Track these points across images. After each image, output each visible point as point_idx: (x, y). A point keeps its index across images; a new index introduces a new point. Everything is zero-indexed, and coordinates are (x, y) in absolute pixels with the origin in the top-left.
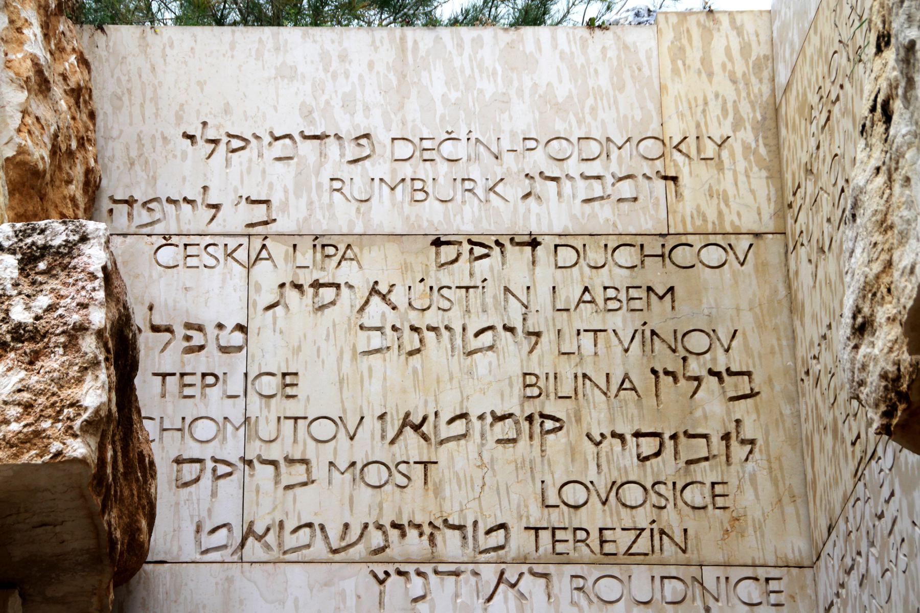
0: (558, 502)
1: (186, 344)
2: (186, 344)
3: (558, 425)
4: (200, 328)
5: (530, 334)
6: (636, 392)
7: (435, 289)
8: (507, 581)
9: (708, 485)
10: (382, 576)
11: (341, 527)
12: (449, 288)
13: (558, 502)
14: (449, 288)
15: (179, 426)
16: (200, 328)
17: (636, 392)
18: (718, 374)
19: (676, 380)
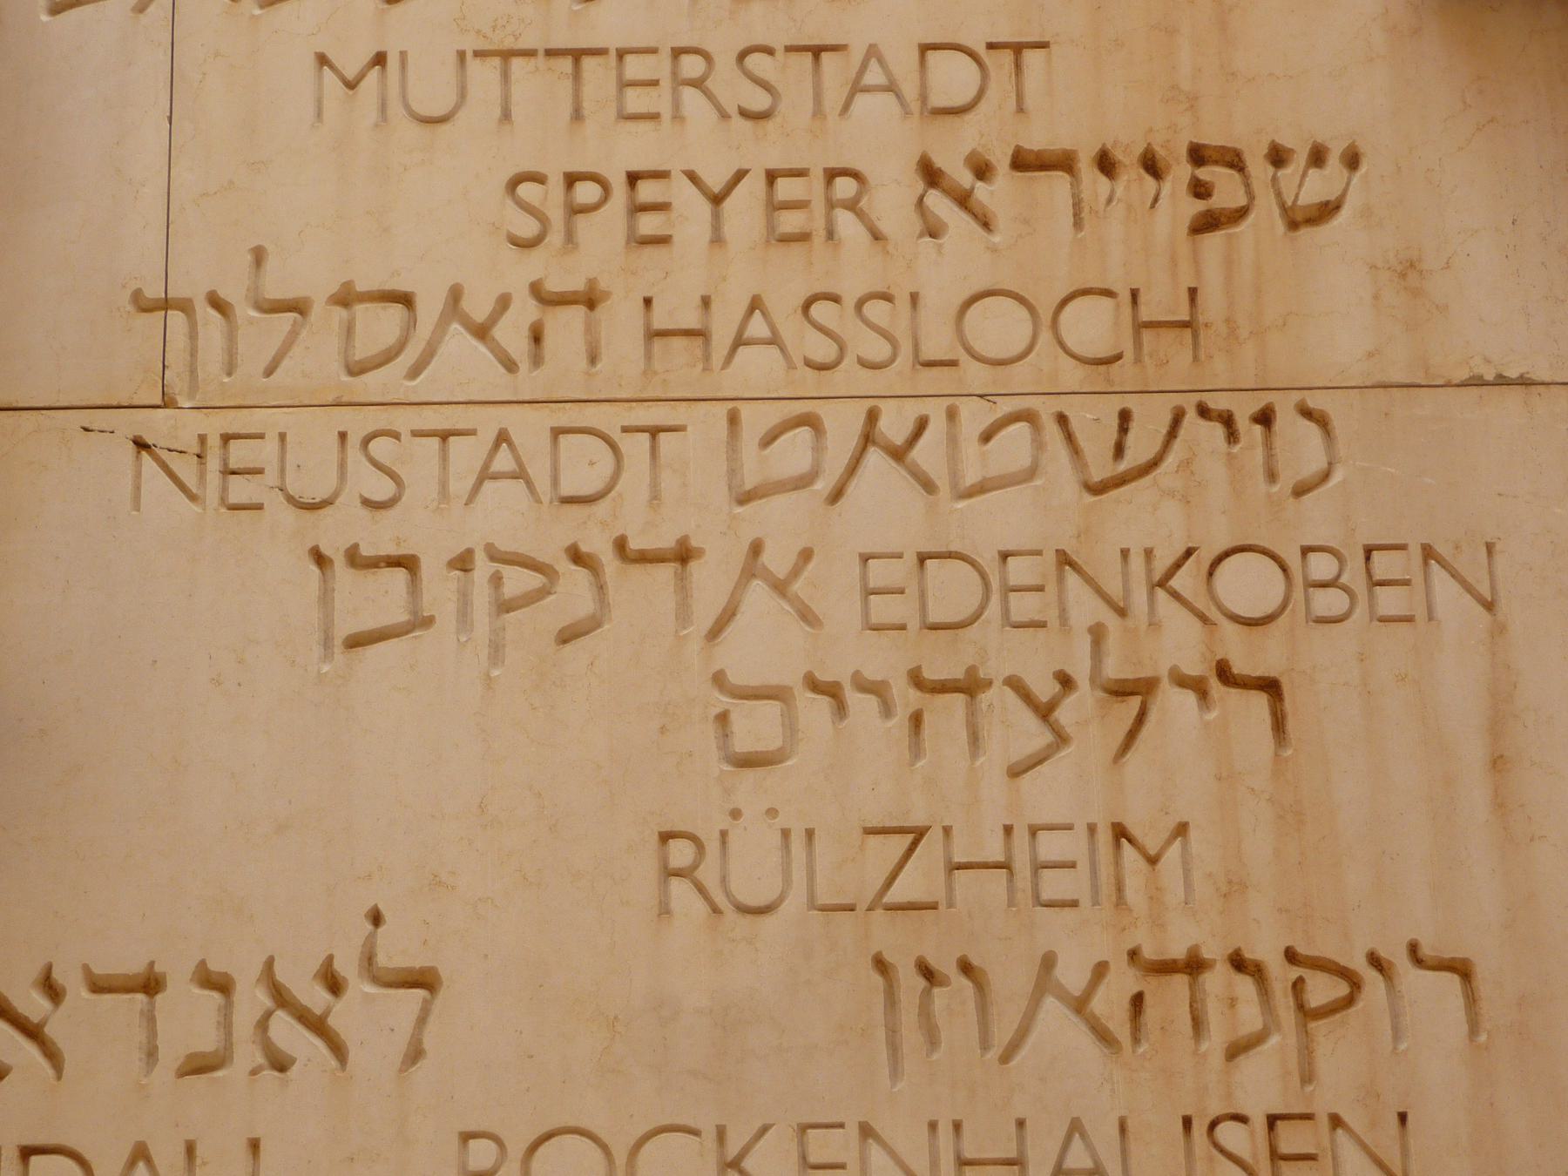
0: (987, 57)
1: (1201, 206)
2: (1201, 206)
3: (1122, 1031)
4: (1234, 161)
5: (1120, 691)
6: (783, 350)
7: (354, 440)
8: (1060, 986)
9: (1259, 1123)
10: (1045, 689)
11: (1013, 1128)
12: (770, 51)
13: (987, 57)
14: (770, 51)
15: (995, 853)
16: (1234, 161)
17: (783, 350)
18: (832, 691)
19: (621, 545)
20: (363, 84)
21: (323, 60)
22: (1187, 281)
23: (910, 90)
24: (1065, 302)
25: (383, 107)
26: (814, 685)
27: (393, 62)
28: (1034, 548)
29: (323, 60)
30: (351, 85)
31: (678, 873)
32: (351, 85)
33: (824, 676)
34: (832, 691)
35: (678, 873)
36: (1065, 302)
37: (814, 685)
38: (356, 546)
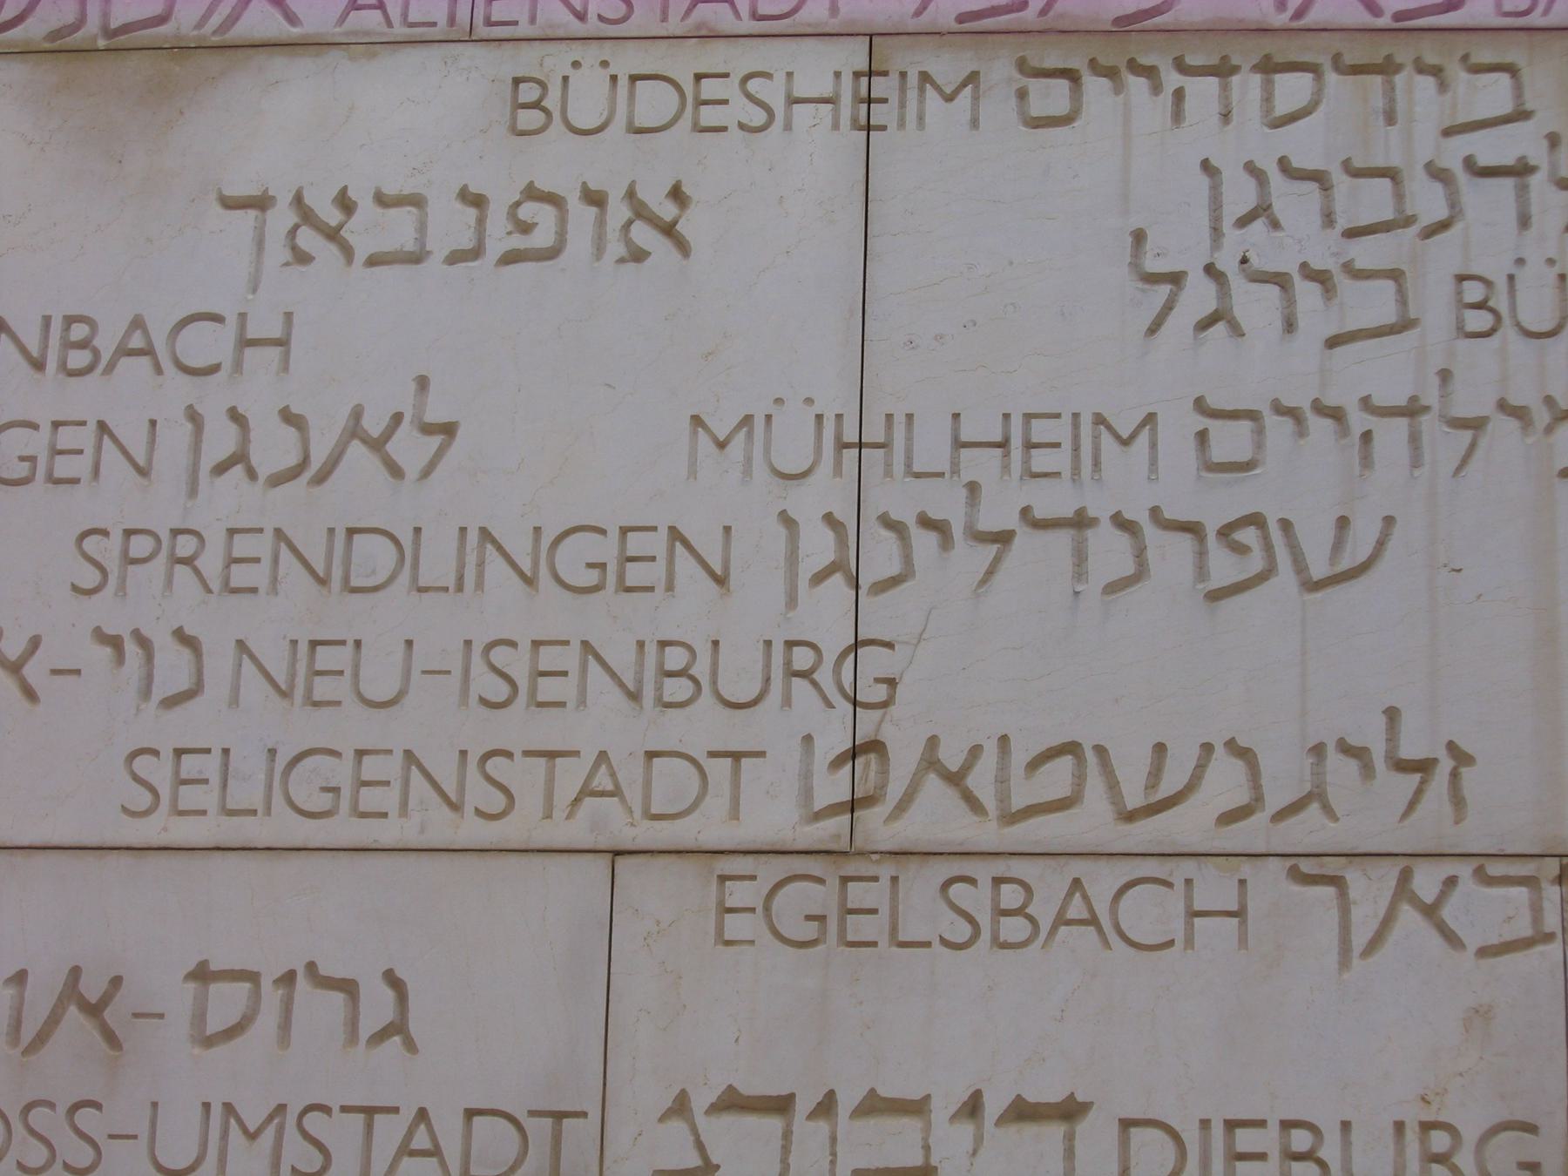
9: (349, 755)
20: (733, 443)
21: (697, 421)
22: (1437, 362)
23: (634, 795)
24: (754, 703)
25: (748, 460)
26: (1279, 409)
27: (759, 423)
28: (887, 639)
29: (697, 421)
30: (722, 445)
31: (798, 674)
32: (722, 445)
33: (1288, 402)
34: (1293, 413)
35: (798, 674)
36: (754, 703)
37: (1279, 409)
38: (465, 186)
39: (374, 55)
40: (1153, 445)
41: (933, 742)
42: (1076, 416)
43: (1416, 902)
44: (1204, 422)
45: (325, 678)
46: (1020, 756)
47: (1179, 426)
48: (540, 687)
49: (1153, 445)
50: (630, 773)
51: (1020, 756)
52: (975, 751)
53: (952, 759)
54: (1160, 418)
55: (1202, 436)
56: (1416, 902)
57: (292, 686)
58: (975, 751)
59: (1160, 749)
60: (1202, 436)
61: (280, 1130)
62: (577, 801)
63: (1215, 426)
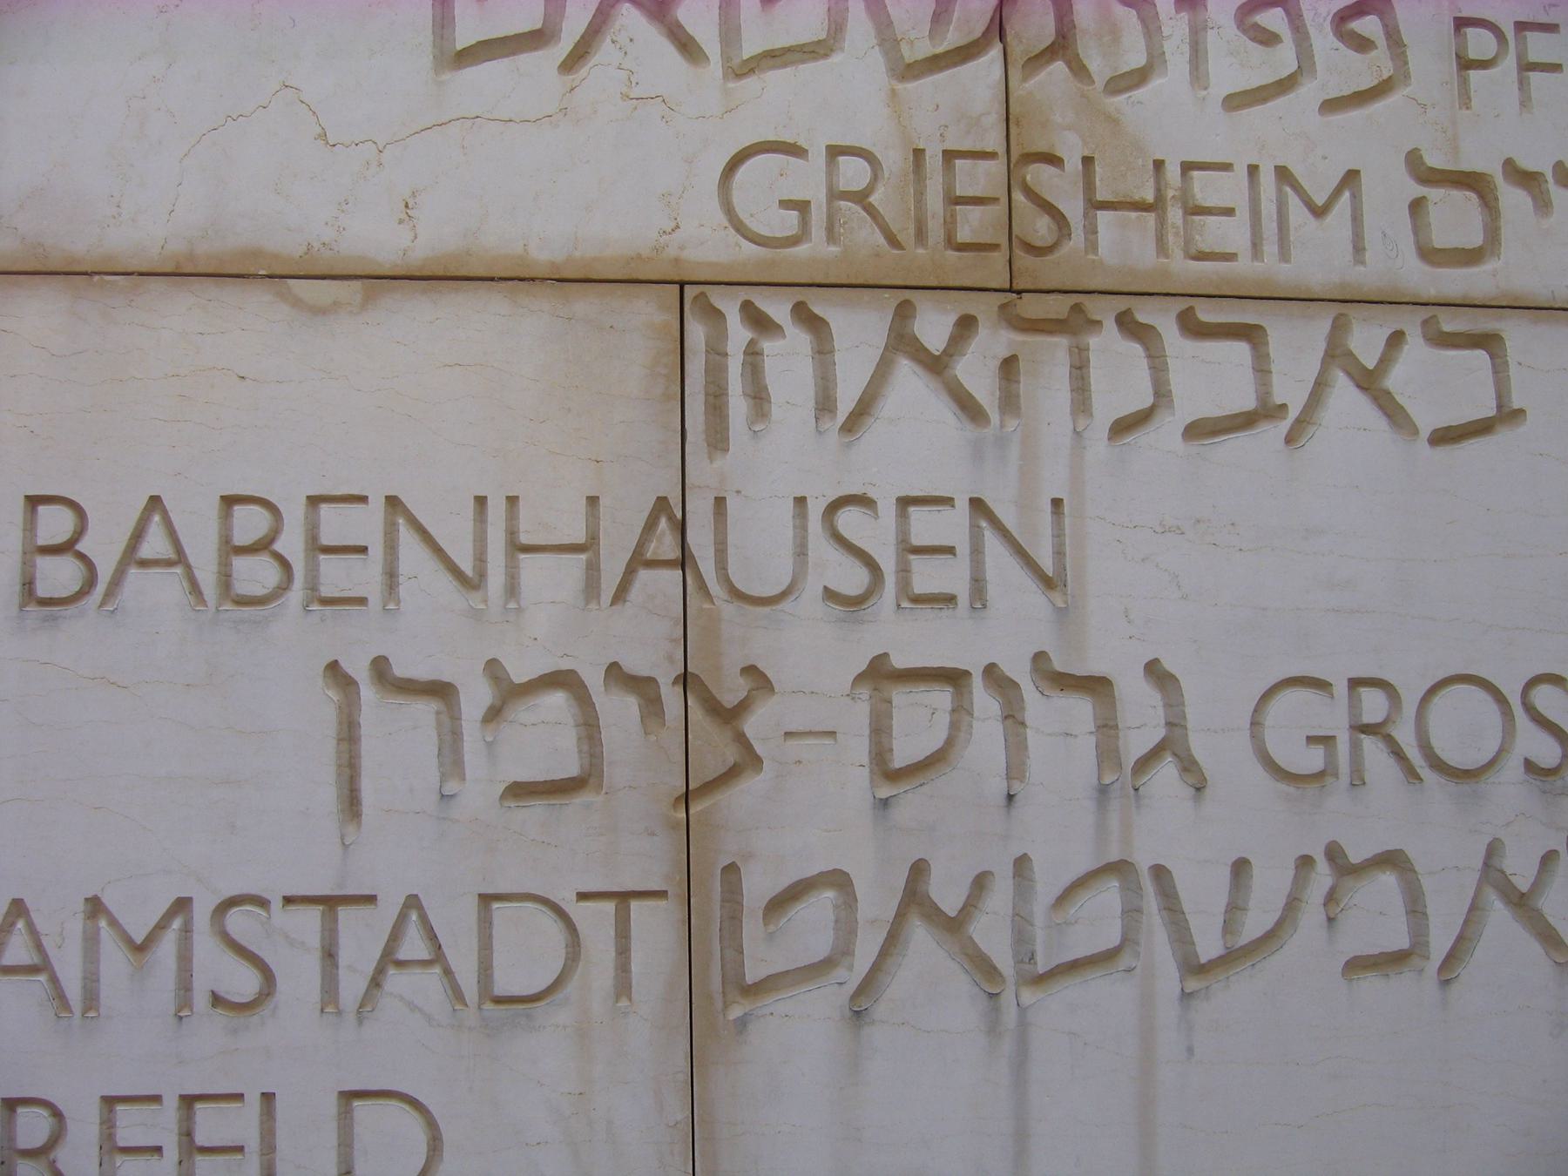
21: (95, 907)
29: (95, 907)
39: (368, 300)
40: (1357, 218)
41: (919, 870)
42: (1253, 170)
43: (934, 914)
44: (1419, 190)
45: (566, 541)
46: (1047, 886)
47: (1389, 189)
48: (281, 551)
49: (1357, 218)
50: (455, 922)
51: (1047, 886)
52: (981, 883)
53: (949, 898)
54: (1364, 178)
55: (1417, 206)
56: (934, 914)
57: (482, 574)
58: (981, 883)
59: (1240, 868)
60: (1417, 206)
61: (187, 930)
62: (376, 982)
63: (1434, 194)
